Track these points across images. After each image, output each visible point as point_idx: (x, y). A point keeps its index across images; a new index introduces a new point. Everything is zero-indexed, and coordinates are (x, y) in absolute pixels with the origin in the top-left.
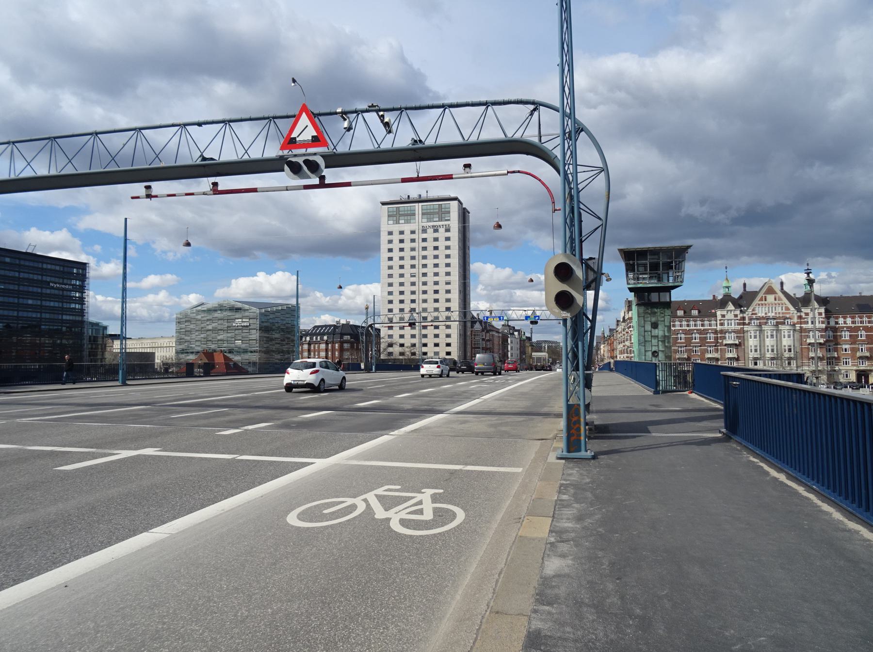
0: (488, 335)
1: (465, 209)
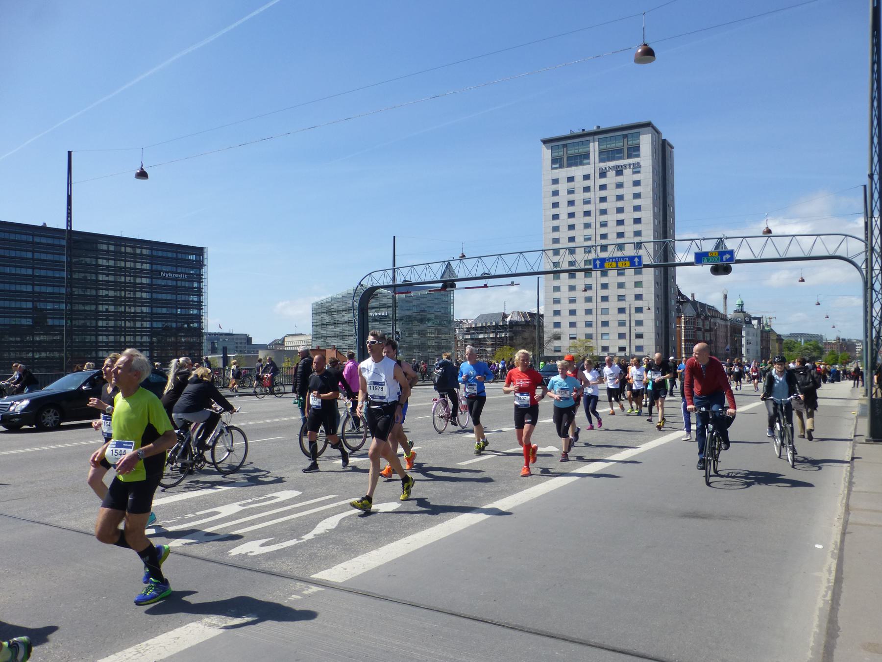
0: (707, 322)
1: (664, 141)
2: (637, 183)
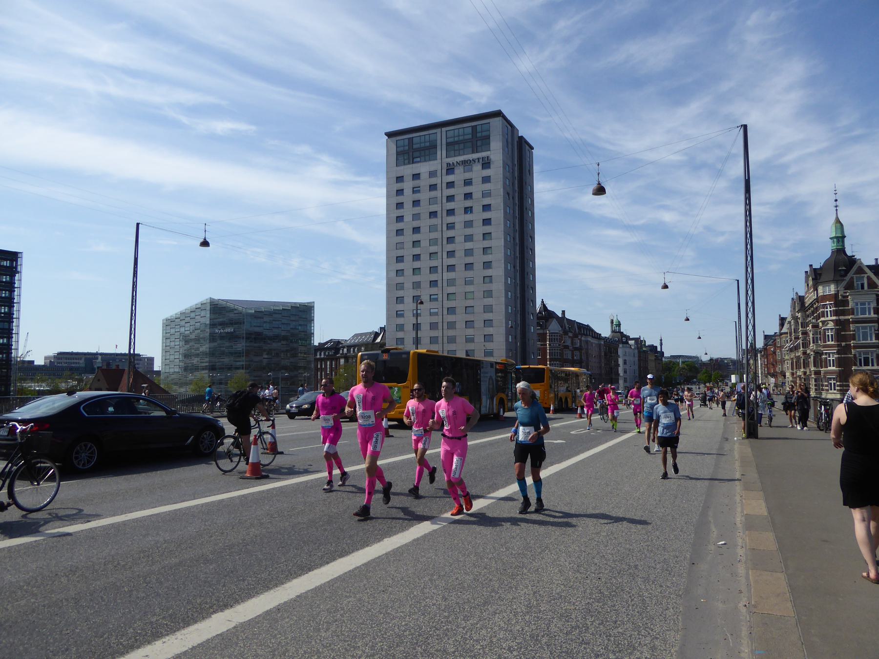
2: (486, 180)
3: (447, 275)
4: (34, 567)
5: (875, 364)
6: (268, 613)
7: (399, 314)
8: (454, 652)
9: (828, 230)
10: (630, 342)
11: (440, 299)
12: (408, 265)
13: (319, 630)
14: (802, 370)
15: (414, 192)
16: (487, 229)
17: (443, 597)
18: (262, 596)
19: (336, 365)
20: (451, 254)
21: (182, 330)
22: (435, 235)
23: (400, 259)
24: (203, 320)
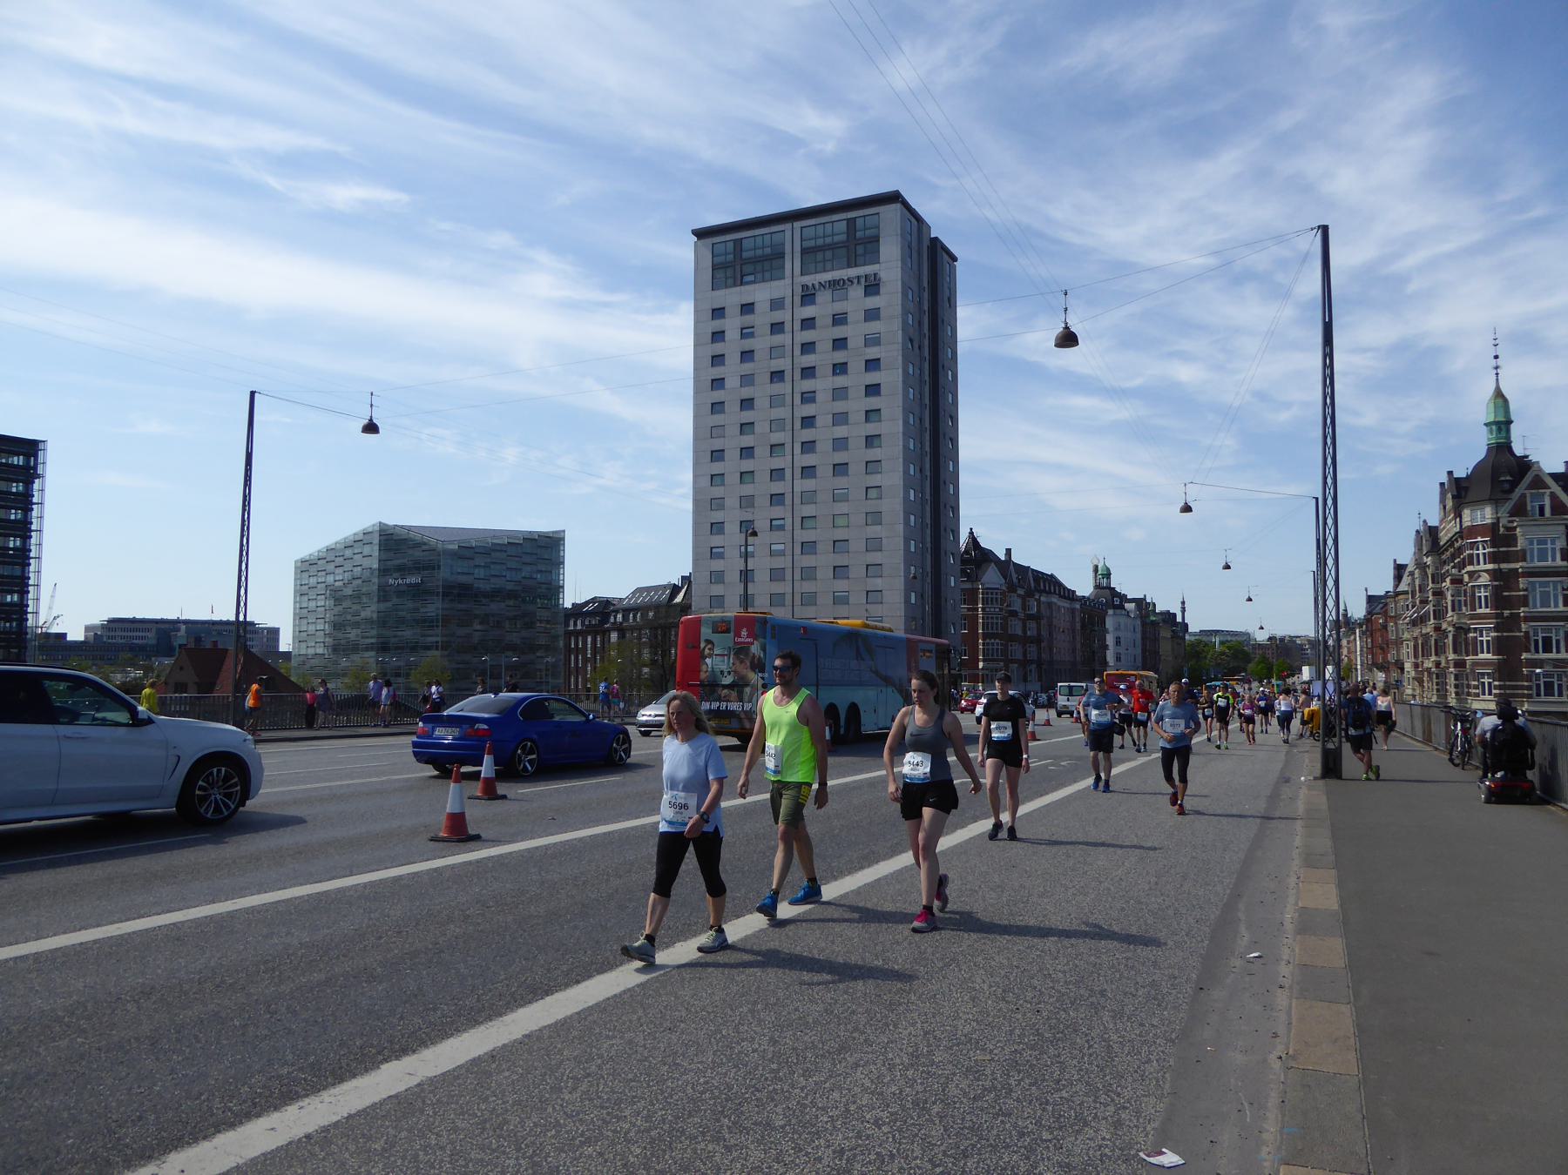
2: (872, 315)
3: (802, 485)
4: (80, 985)
5: (1563, 649)
6: (475, 1061)
7: (715, 554)
8: (783, 1127)
9: (1480, 411)
10: (1127, 606)
11: (788, 527)
12: (732, 465)
13: (560, 1090)
14: (1433, 658)
15: (743, 336)
16: (873, 402)
17: (772, 1039)
18: (465, 1035)
19: (603, 642)
20: (808, 447)
21: (330, 579)
22: (782, 412)
23: (717, 455)
24: (367, 563)
